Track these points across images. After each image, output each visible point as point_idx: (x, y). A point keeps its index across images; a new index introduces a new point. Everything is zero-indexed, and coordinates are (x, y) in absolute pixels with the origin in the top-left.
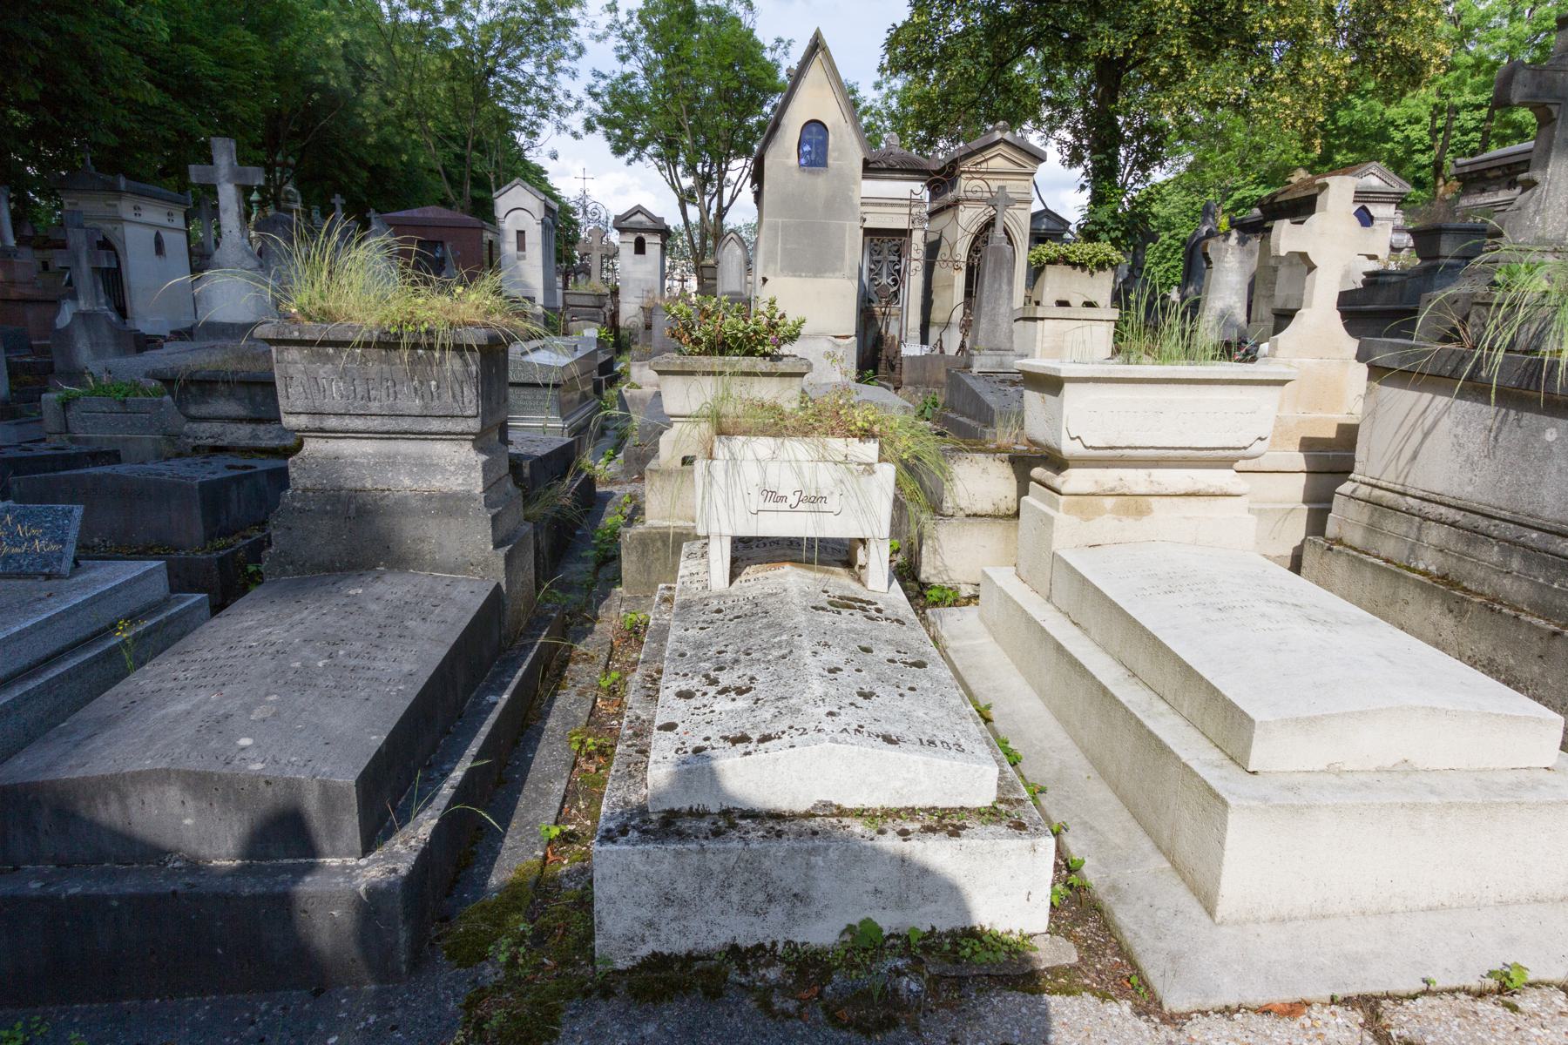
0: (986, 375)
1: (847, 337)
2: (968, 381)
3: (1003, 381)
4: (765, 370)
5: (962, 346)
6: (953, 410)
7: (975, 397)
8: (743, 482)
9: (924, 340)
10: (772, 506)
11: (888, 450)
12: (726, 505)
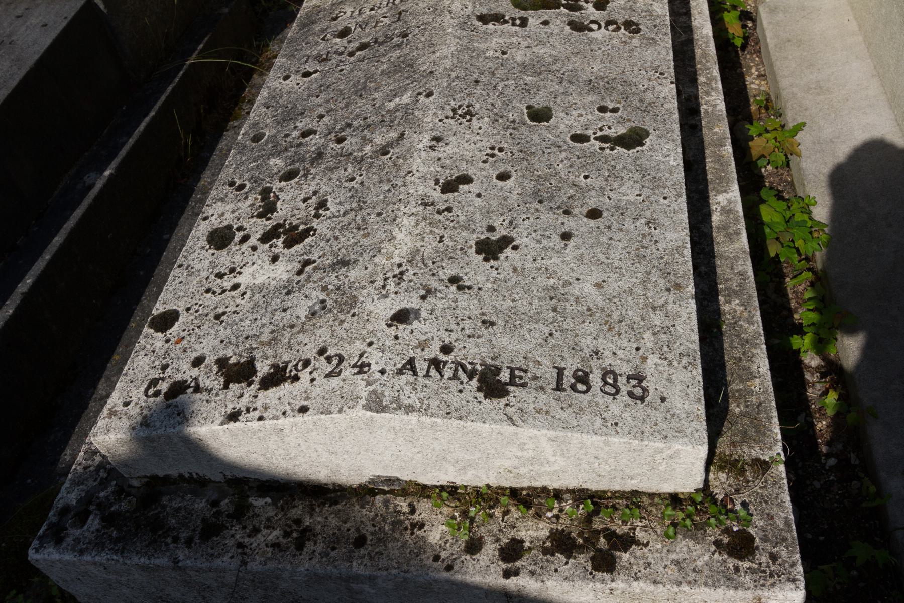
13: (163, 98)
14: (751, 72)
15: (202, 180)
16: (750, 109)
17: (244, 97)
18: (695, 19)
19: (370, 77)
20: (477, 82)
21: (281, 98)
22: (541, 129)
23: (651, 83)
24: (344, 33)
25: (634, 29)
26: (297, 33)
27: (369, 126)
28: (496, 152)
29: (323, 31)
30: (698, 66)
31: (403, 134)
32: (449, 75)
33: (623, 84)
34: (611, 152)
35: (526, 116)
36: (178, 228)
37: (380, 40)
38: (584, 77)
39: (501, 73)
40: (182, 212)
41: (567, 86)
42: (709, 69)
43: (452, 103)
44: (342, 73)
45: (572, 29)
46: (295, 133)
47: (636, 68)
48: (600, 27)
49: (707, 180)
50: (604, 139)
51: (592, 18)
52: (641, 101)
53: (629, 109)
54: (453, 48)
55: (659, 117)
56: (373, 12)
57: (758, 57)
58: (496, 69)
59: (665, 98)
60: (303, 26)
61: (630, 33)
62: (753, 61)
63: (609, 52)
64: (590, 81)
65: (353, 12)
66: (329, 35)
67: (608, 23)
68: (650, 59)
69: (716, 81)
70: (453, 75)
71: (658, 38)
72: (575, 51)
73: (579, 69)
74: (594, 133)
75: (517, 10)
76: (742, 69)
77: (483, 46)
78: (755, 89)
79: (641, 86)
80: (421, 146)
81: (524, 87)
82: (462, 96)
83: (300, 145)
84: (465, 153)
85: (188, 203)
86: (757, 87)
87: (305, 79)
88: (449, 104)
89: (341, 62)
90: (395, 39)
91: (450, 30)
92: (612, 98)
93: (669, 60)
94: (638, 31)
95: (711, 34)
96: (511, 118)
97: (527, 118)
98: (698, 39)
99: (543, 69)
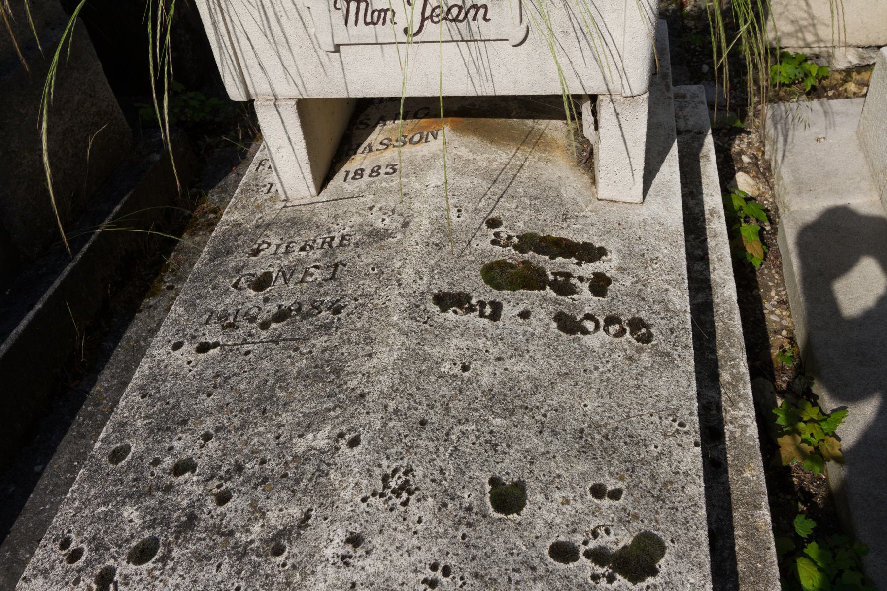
10: (363, 32)
13: (57, 283)
14: (769, 295)
15: (98, 383)
16: (770, 354)
17: (168, 265)
18: (714, 269)
19: (281, 378)
20: (423, 423)
21: (164, 381)
22: (509, 528)
23: (667, 442)
24: (262, 283)
25: (643, 335)
26: (206, 265)
27: (266, 479)
28: (439, 574)
29: (238, 270)
30: (720, 352)
31: (307, 516)
32: (386, 406)
33: (628, 440)
34: (609, 586)
35: (487, 500)
36: (55, 457)
37: (306, 308)
38: (573, 425)
39: (458, 405)
40: (64, 432)
41: (549, 439)
42: (734, 359)
43: (385, 463)
44: (247, 358)
45: (560, 328)
46: (168, 462)
47: (646, 411)
48: (597, 327)
49: (737, 573)
50: (598, 556)
51: (587, 310)
52: (653, 477)
53: (637, 494)
54: (396, 353)
55: (678, 514)
56: (303, 253)
57: (777, 273)
58: (452, 399)
59: (686, 474)
60: (216, 254)
61: (638, 340)
62: (772, 278)
63: (609, 375)
64: (582, 431)
65: (279, 246)
66: (243, 280)
67: (611, 320)
68: (665, 394)
69: (745, 383)
70: (392, 406)
71: (675, 354)
72: (564, 370)
73: (567, 406)
74: (586, 543)
75: (488, 288)
76: (759, 290)
77: (436, 352)
78: (775, 322)
79: (653, 447)
80: (329, 552)
81: (488, 437)
82: (400, 449)
83: (169, 488)
84: (393, 574)
85: (74, 417)
86: (777, 319)
87: (201, 356)
88: (380, 466)
89: (251, 335)
90: (323, 314)
91: (395, 318)
92: (612, 469)
93: (691, 399)
94: (647, 339)
95: (735, 298)
96: (466, 502)
97: (489, 504)
98: (718, 304)
99: (518, 403)
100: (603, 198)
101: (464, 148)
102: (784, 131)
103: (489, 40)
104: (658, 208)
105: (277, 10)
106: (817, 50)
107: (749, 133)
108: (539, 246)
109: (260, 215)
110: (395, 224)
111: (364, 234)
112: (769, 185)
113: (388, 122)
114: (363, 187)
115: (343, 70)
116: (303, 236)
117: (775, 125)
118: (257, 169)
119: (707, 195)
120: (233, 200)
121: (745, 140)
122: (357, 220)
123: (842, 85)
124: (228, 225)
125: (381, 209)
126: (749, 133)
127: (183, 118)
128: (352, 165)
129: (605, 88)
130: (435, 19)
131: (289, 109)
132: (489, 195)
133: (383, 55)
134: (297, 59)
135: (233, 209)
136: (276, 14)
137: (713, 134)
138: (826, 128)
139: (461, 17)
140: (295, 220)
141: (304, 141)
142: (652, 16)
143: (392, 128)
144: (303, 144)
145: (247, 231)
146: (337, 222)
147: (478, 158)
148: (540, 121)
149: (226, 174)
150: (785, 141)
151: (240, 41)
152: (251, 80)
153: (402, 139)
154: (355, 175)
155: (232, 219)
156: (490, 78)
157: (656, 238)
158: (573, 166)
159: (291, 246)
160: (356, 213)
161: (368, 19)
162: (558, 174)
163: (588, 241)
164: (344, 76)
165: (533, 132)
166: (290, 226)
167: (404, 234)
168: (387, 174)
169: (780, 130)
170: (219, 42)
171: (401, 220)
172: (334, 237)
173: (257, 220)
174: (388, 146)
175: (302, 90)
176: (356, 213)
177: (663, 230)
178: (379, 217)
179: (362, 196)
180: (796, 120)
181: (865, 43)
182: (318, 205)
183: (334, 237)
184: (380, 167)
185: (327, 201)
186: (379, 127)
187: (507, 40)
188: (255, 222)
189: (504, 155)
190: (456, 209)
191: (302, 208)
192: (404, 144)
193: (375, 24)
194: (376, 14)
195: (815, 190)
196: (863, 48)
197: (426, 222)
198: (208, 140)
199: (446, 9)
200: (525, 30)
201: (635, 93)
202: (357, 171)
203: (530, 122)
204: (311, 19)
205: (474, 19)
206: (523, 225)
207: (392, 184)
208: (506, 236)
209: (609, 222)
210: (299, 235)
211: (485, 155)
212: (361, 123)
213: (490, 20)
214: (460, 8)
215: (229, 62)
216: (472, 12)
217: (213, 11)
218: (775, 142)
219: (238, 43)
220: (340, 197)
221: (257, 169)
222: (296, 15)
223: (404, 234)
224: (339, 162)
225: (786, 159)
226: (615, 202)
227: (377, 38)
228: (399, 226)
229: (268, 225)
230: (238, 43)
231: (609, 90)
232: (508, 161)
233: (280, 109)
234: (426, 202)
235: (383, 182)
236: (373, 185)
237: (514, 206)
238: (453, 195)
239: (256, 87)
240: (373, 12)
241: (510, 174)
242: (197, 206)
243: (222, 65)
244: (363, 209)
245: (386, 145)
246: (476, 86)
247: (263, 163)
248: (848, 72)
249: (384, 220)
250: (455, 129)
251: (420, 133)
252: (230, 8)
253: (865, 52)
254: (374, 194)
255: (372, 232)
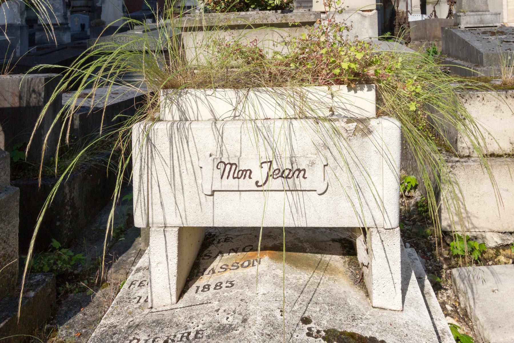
0: (471, 29)
1: (371, 11)
2: (459, 34)
3: (484, 33)
4: (276, 21)
5: (450, 13)
6: (449, 55)
7: (465, 44)
8: (193, 151)
9: (423, 11)
10: (231, 183)
11: (389, 99)
12: (172, 184)
100: (376, 306)
101: (279, 270)
102: (470, 285)
103: (305, 191)
104: (414, 315)
105: (182, 168)
106: (474, 234)
107: (446, 290)
108: (340, 337)
109: (132, 319)
110: (237, 321)
111: (213, 329)
112: (470, 328)
113: (225, 255)
114: (210, 296)
115: (213, 207)
116: (166, 332)
117: (463, 281)
118: (129, 287)
119: (436, 319)
120: (110, 309)
121: (445, 294)
122: (207, 319)
123: (496, 258)
124: (106, 327)
125: (225, 311)
126: (446, 290)
127: (55, 267)
128: (201, 282)
129: (374, 224)
130: (275, 177)
131: (172, 234)
132: (300, 302)
133: (240, 199)
134: (186, 200)
135: (110, 316)
136: (180, 171)
137: (428, 278)
138: (496, 283)
139: (290, 176)
140: (159, 321)
141: (177, 258)
142: (398, 179)
143: (228, 258)
144: (176, 260)
145: (120, 331)
146: (192, 321)
147: (289, 277)
148: (325, 255)
149: (75, 313)
150: (472, 291)
151: (153, 187)
152: (152, 213)
153: (236, 264)
154: (204, 289)
155: (109, 322)
156: (304, 215)
157: (418, 335)
158: (352, 284)
159: (156, 340)
160: (206, 314)
161: (235, 176)
162: (343, 289)
163: (373, 336)
164: (213, 211)
165: (322, 262)
166: (156, 326)
167: (244, 327)
168: (227, 287)
169: (467, 285)
170: (140, 187)
171: (241, 317)
172: (191, 332)
173: (129, 323)
174: (226, 269)
175: (184, 221)
176: (206, 314)
177: (421, 330)
178: (224, 317)
179: (210, 303)
180: (476, 278)
181: (501, 230)
182: (176, 310)
183: (191, 332)
184: (221, 283)
185: (184, 307)
186: (218, 258)
187: (316, 191)
188: (127, 324)
189: (306, 275)
190: (279, 310)
191: (164, 313)
192: (238, 267)
193: (239, 178)
194: (241, 172)
195: (503, 327)
196: (501, 233)
197: (259, 318)
198: (67, 286)
199: (281, 171)
200: (327, 184)
201: (393, 226)
202: (205, 286)
203: (319, 256)
204: (200, 174)
205: (297, 177)
206: (326, 323)
207: (231, 294)
208: (316, 331)
209: (384, 323)
210: (162, 332)
211: (293, 275)
212: (206, 255)
213: (306, 178)
214: (290, 170)
215: (143, 200)
216: (297, 173)
217: (143, 167)
218: (466, 293)
219: (152, 188)
220: (193, 304)
221: (129, 287)
222: (192, 172)
223: (244, 327)
224: (191, 280)
225: (477, 305)
226: (384, 309)
227: (239, 187)
228: (240, 322)
229: (138, 325)
230: (152, 188)
231: (376, 225)
232: (308, 279)
233: (167, 234)
234: (258, 305)
235: (224, 292)
236: (218, 295)
237: (318, 309)
238: (276, 300)
239: (154, 218)
240: (239, 171)
241: (312, 288)
242: (48, 339)
243: (137, 202)
244: (211, 312)
245: (224, 269)
246: (295, 220)
247: (134, 283)
248: (497, 248)
249: (228, 318)
250: (272, 258)
251: (248, 261)
252: (153, 167)
253: (503, 235)
254: (219, 301)
255: (219, 327)
